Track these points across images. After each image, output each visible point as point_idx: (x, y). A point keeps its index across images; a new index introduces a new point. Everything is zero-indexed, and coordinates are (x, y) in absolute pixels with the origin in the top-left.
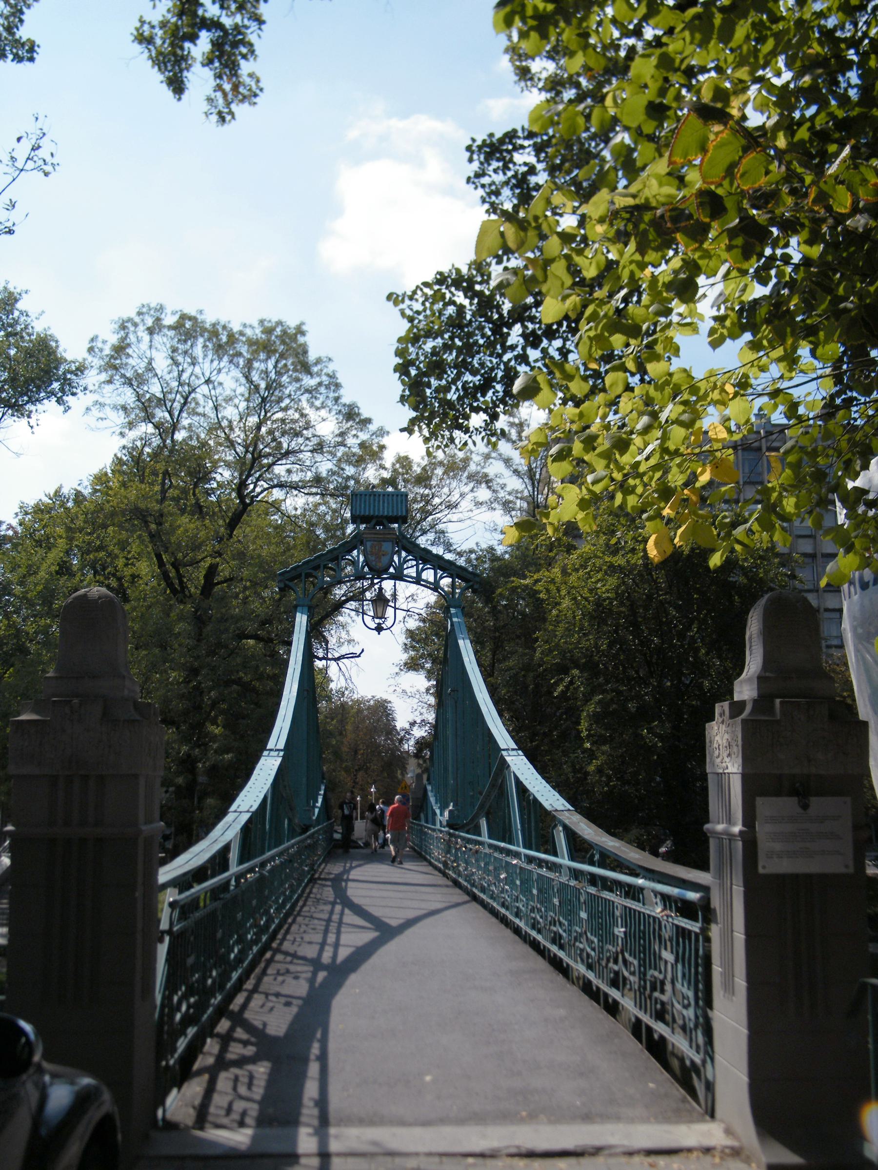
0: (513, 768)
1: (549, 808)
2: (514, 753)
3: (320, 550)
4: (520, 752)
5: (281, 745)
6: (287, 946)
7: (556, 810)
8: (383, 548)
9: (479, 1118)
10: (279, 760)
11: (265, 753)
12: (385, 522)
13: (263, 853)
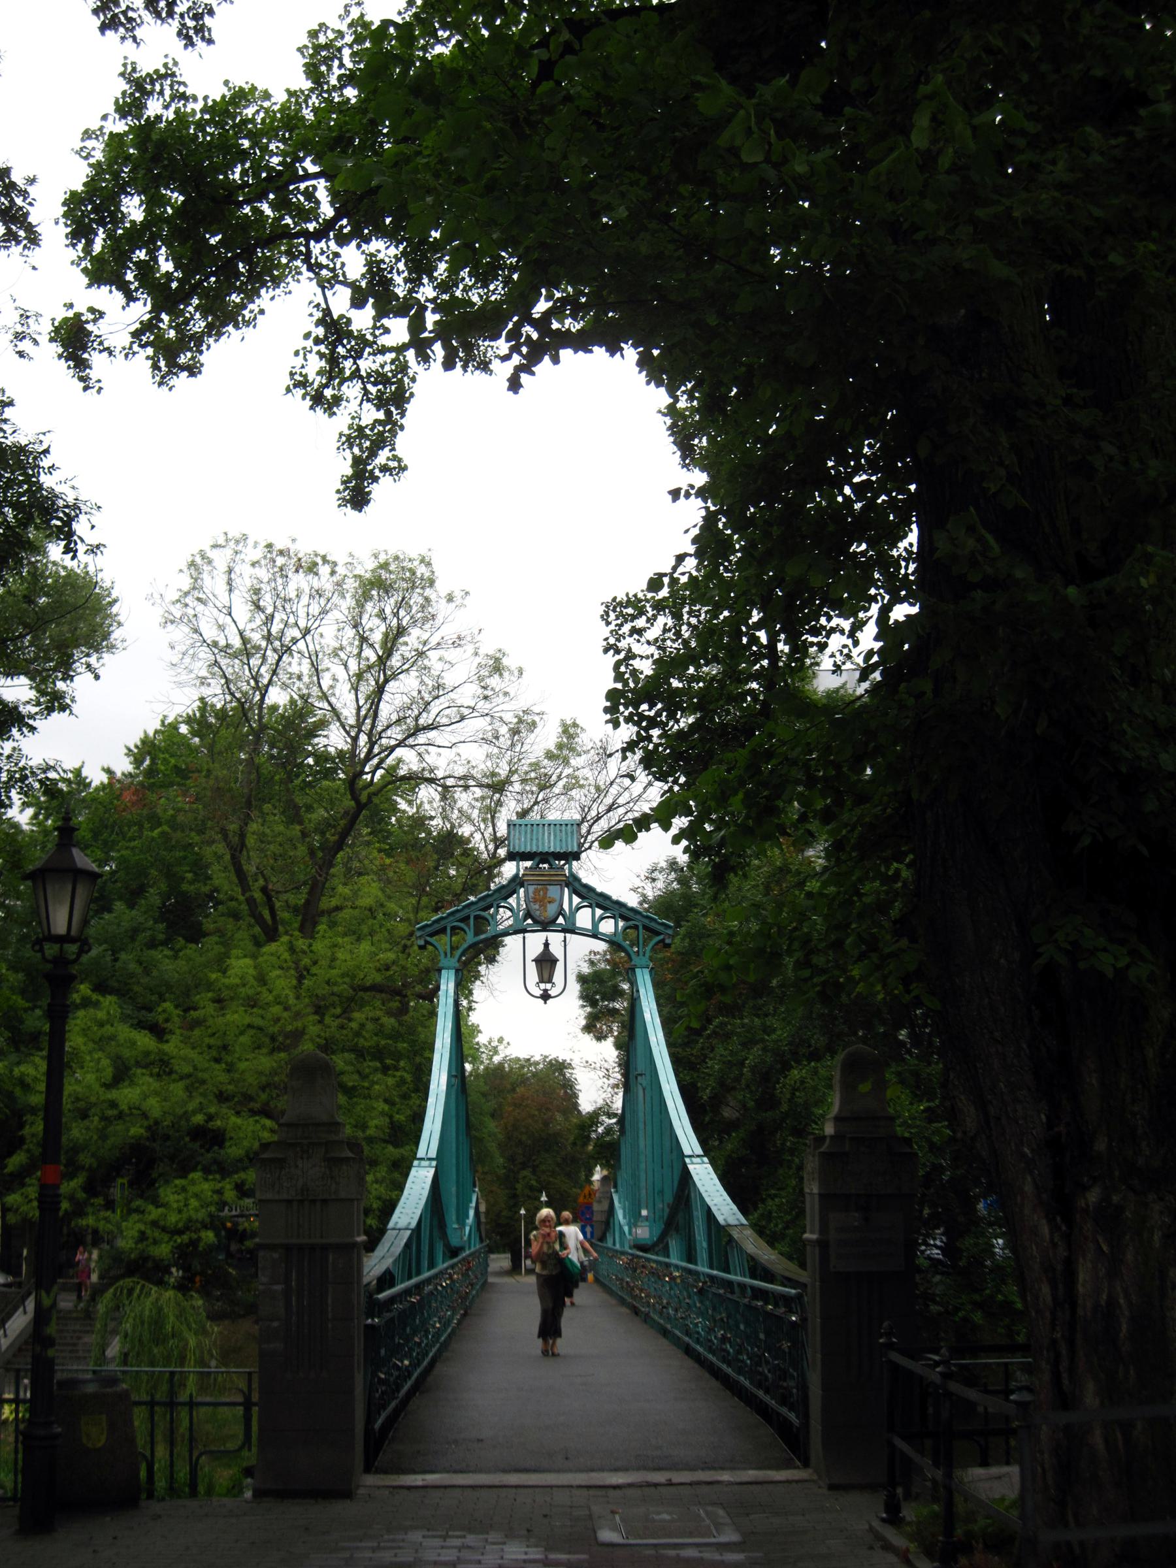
2: (698, 1160)
4: (706, 1159)
5: (433, 1153)
7: (729, 1225)
9: (625, 1469)
10: (432, 1171)
11: (416, 1163)
13: (418, 1273)
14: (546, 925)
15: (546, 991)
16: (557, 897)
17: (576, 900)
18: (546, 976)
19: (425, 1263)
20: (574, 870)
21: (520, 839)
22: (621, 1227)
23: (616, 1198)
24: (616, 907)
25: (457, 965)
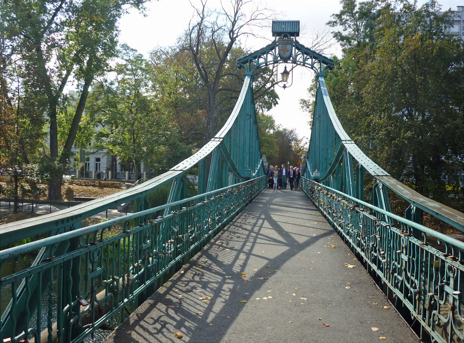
0: (349, 150)
1: (373, 174)
2: (349, 142)
3: (333, 174)
6: (213, 252)
7: (378, 176)
8: (287, 48)
12: (288, 35)
14: (285, 60)
15: (285, 85)
16: (290, 49)
17: (297, 51)
18: (285, 78)
19: (260, 175)
20: (297, 40)
21: (277, 27)
22: (309, 172)
23: (308, 162)
24: (312, 53)
25: (251, 74)
